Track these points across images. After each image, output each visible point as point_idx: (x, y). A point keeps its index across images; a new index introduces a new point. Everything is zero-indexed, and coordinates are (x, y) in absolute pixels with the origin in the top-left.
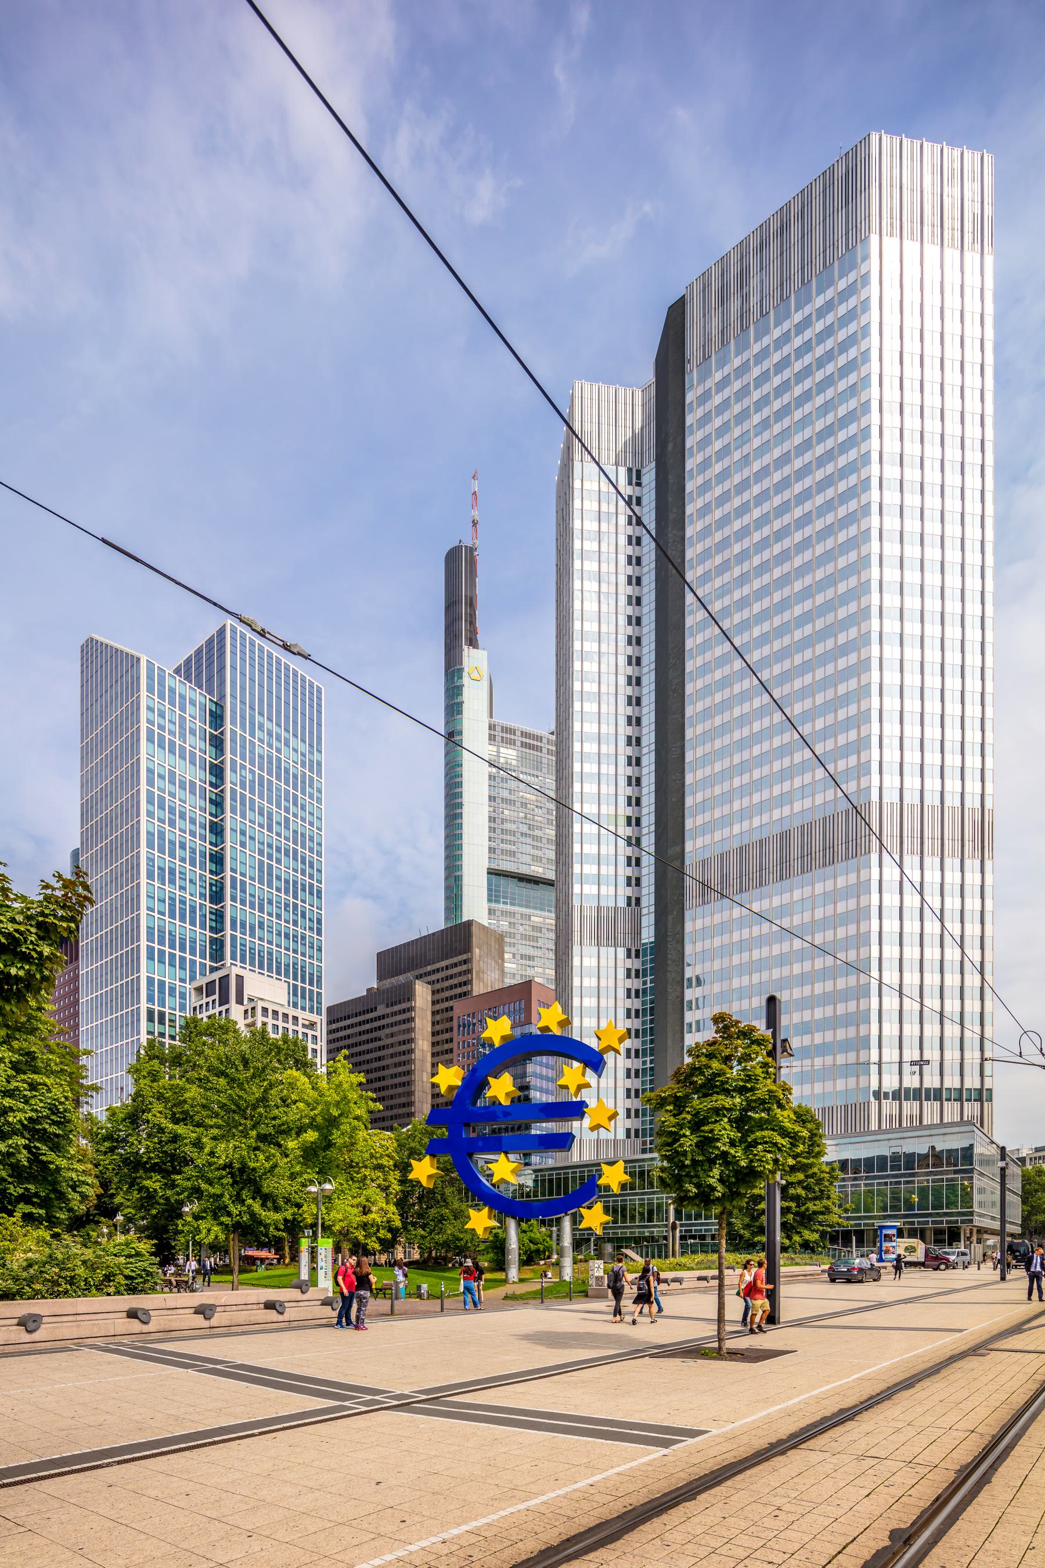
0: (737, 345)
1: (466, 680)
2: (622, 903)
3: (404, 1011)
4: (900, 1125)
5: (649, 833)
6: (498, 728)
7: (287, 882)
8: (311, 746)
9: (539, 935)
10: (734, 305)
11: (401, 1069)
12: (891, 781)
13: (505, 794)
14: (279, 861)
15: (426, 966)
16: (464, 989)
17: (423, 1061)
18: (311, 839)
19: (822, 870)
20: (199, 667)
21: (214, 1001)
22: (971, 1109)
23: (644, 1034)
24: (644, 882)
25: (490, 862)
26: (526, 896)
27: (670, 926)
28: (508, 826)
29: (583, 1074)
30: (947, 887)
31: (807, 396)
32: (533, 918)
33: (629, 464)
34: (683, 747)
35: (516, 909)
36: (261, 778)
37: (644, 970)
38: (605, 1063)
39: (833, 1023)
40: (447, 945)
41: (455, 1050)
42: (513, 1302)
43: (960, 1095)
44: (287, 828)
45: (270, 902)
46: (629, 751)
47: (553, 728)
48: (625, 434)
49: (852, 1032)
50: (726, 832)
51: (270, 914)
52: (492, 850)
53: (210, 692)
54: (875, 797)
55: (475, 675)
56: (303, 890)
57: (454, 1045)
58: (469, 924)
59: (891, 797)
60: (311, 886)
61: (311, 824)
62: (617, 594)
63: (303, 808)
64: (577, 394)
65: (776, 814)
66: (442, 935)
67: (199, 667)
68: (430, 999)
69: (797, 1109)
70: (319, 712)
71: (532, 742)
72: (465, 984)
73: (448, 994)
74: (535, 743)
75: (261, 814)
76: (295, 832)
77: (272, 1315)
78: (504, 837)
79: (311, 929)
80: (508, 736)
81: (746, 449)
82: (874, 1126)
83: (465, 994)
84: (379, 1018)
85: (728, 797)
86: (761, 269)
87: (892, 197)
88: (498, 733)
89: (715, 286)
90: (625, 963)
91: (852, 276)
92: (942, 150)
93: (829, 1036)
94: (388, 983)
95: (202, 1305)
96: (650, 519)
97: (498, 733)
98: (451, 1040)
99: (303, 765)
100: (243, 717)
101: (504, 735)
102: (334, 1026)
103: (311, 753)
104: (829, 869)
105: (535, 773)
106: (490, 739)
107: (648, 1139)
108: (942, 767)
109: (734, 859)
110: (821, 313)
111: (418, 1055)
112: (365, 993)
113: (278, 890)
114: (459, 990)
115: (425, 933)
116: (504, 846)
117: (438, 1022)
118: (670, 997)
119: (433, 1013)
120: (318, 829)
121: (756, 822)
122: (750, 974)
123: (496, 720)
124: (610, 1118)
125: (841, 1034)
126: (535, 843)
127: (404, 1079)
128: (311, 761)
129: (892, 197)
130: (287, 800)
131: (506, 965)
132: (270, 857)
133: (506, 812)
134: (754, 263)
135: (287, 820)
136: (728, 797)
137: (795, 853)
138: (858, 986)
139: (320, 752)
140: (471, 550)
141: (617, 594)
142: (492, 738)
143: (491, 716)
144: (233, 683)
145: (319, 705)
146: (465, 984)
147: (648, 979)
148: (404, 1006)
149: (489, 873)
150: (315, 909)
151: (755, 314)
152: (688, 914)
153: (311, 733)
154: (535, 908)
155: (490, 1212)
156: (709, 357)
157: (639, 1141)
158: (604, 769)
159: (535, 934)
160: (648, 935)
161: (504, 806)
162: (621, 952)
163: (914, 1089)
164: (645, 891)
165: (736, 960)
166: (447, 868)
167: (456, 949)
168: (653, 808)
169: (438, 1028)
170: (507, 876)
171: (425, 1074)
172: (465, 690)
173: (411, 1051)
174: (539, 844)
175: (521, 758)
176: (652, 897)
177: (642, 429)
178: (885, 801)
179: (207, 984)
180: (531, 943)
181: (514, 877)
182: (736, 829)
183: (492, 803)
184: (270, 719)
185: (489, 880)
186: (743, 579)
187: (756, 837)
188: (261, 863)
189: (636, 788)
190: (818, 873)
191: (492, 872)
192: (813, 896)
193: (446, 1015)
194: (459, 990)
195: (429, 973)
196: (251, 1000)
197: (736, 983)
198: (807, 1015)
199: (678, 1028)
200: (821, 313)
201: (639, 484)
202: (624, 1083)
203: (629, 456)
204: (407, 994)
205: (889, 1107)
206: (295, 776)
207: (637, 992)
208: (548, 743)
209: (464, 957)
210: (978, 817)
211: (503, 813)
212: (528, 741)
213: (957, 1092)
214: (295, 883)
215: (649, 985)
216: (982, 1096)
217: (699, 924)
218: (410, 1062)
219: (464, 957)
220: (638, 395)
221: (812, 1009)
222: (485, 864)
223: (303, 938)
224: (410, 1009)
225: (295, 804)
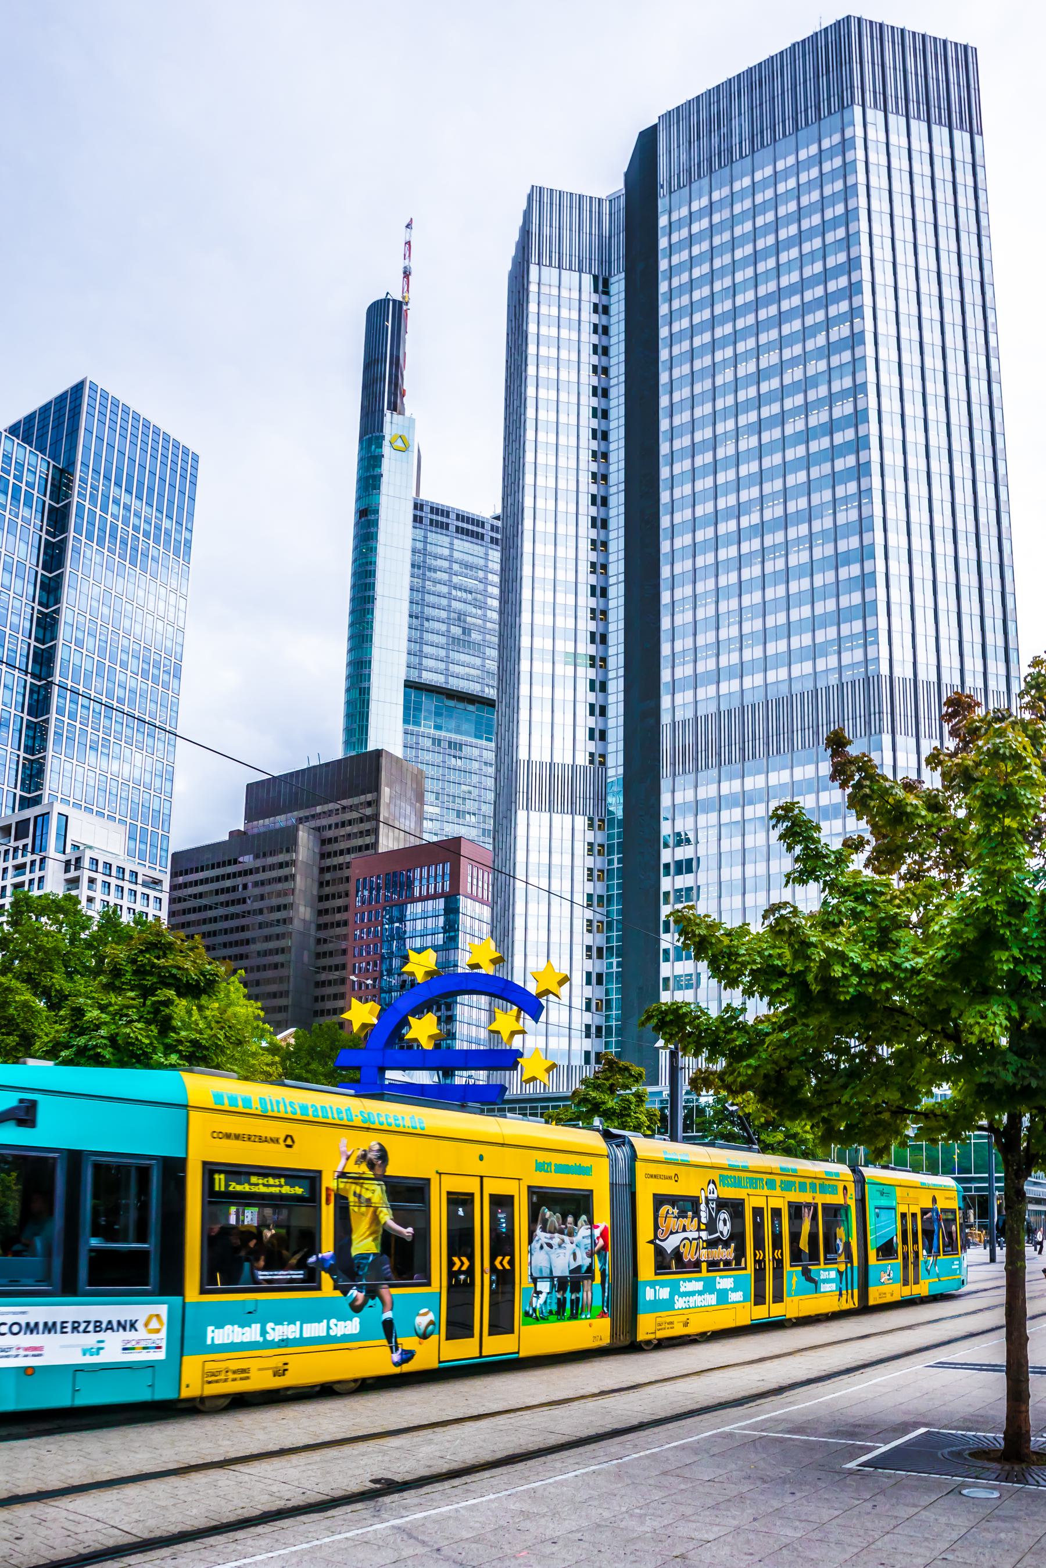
1: (386, 450)
2: (582, 760)
3: (281, 866)
6: (427, 509)
11: (272, 945)
15: (315, 806)
20: (43, 427)
21: (25, 846)
23: (610, 877)
24: (611, 735)
33: (595, 270)
46: (591, 722)
53: (55, 457)
54: (884, 670)
58: (378, 753)
62: (578, 404)
67: (43, 427)
83: (367, 847)
84: (240, 874)
90: (585, 836)
94: (263, 824)
102: (181, 880)
112: (227, 838)
115: (314, 762)
124: (561, 983)
141: (578, 404)
148: (282, 858)
149: (406, 686)
158: (560, 598)
162: (581, 821)
164: (612, 699)
172: (385, 462)
179: (17, 823)
189: (601, 647)
191: (409, 685)
196: (76, 847)
202: (582, 1018)
204: (287, 840)
212: (465, 525)
215: (615, 969)
222: (401, 674)
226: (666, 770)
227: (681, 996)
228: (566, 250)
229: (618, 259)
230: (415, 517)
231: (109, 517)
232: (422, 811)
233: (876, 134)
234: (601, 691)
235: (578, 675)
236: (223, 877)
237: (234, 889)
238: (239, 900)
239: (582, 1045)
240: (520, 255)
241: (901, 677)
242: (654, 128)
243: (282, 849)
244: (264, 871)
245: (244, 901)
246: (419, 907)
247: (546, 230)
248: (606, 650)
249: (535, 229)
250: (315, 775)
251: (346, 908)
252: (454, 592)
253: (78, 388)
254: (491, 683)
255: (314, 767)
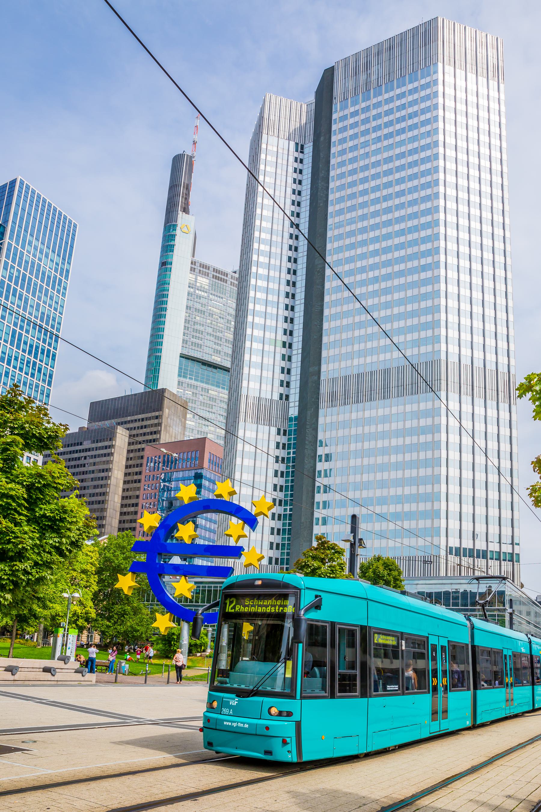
0: (363, 96)
1: (178, 232)
2: (276, 397)
3: (106, 447)
4: (460, 574)
5: (297, 354)
7: (31, 346)
8: (64, 259)
9: (214, 404)
10: (362, 78)
12: (453, 349)
13: (198, 306)
14: (27, 332)
15: (127, 416)
16: (154, 437)
17: (117, 486)
18: (54, 319)
19: (410, 397)
22: (506, 566)
25: (182, 349)
26: (207, 376)
27: (308, 418)
28: (197, 327)
29: (243, 529)
30: (488, 419)
31: (402, 131)
32: (210, 391)
34: (322, 306)
35: (199, 384)
36: (24, 276)
37: (289, 445)
38: (258, 522)
39: (417, 498)
40: (145, 404)
41: (143, 481)
42: (188, 682)
43: (498, 556)
44: (38, 310)
45: (16, 359)
47: (237, 268)
48: (295, 125)
49: (429, 506)
50: (349, 363)
51: (15, 367)
52: (185, 342)
54: (443, 357)
55: (185, 230)
56: (43, 353)
57: (142, 477)
58: (163, 390)
59: (453, 359)
60: (49, 351)
61: (56, 309)
63: (51, 298)
64: (267, 100)
65: (382, 357)
66: (142, 396)
68: (127, 440)
69: (386, 561)
70: (73, 239)
71: (220, 276)
72: (155, 433)
73: (140, 439)
74: (223, 277)
75: (20, 298)
76: (43, 314)
77: (48, 676)
78: (195, 334)
79: (44, 381)
80: (204, 270)
81: (367, 149)
82: (443, 573)
83: (154, 440)
84: (83, 451)
85: (351, 341)
86: (378, 64)
87: (449, 47)
88: (197, 268)
89: (351, 65)
90: (275, 438)
91: (428, 79)
92: (476, 31)
93: (414, 507)
95: (10, 666)
96: (304, 227)
97: (197, 268)
98: (140, 473)
99: (56, 270)
100: (18, 236)
101: (201, 269)
103: (63, 264)
104: (415, 397)
105: (221, 295)
106: (191, 270)
107: (285, 566)
108: (484, 345)
109: (353, 381)
110: (411, 92)
111: (113, 481)
112: (77, 431)
113: (24, 351)
114: (150, 437)
115: (129, 393)
116: (194, 340)
117: (131, 459)
118: (306, 467)
119: (128, 451)
120: (60, 313)
121: (369, 360)
122: (362, 458)
123: (196, 259)
125: (422, 507)
126: (217, 341)
127: (100, 498)
128: (62, 269)
129: (449, 47)
130: (40, 292)
131: (187, 422)
132: (21, 328)
133: (198, 318)
134: (374, 61)
135: (38, 305)
136: (351, 341)
137: (394, 383)
138: (433, 475)
139: (69, 263)
140: (191, 158)
142: (192, 270)
143: (193, 256)
144: (16, 214)
145: (74, 235)
146: (155, 433)
147: (292, 451)
149: (181, 357)
150: (49, 367)
151: (374, 84)
152: (321, 412)
153: (65, 251)
154: (212, 385)
155: (170, 616)
156: (347, 99)
157: (279, 566)
159: (211, 403)
160: (294, 412)
161: (197, 314)
162: (274, 430)
163: (469, 549)
164: (294, 365)
165: (353, 447)
166: (150, 349)
167: (151, 407)
168: (301, 339)
169: (131, 462)
170: (194, 360)
171: (116, 496)
172: (177, 238)
173: (107, 478)
174: (219, 342)
175: (212, 285)
176: (298, 396)
177: (306, 124)
178: (449, 360)
180: (208, 409)
181: (200, 362)
182: (356, 362)
183: (189, 311)
184: (37, 239)
185: (180, 363)
186: (364, 217)
187: (368, 369)
188: (14, 332)
190: (408, 398)
191: (182, 356)
192: (405, 413)
193: (138, 454)
194: (150, 437)
195: (129, 422)
197: (352, 463)
198: (399, 491)
199: (310, 489)
200: (411, 92)
201: (302, 152)
202: (268, 538)
203: (297, 137)
204: (111, 435)
205: (453, 559)
206: (49, 277)
207: (283, 459)
208: (232, 278)
209: (157, 414)
210: (506, 378)
211: (195, 318)
213: (497, 554)
214: (37, 348)
215: (292, 455)
216: (513, 558)
217: (328, 420)
218: (106, 486)
219: (157, 414)
220: (304, 107)
221: (403, 487)
223: (37, 386)
224: (111, 447)
225: (46, 295)
226: (323, 404)
227: (325, 539)
228: (282, 128)
229: (310, 135)
230: (191, 268)
231: (25, 252)
232: (185, 423)
233: (449, 79)
234: (288, 361)
235: (276, 351)
236: (74, 452)
237: (79, 459)
238: (81, 465)
239: (268, 553)
240: (258, 129)
241: (452, 361)
242: (332, 68)
243: (107, 438)
244: (96, 450)
245: (84, 466)
246: (181, 474)
247: (272, 117)
248: (292, 352)
249: (266, 116)
250: (128, 400)
251: (140, 473)
252: (211, 296)
253: (13, 183)
254: (221, 413)
255: (129, 396)
